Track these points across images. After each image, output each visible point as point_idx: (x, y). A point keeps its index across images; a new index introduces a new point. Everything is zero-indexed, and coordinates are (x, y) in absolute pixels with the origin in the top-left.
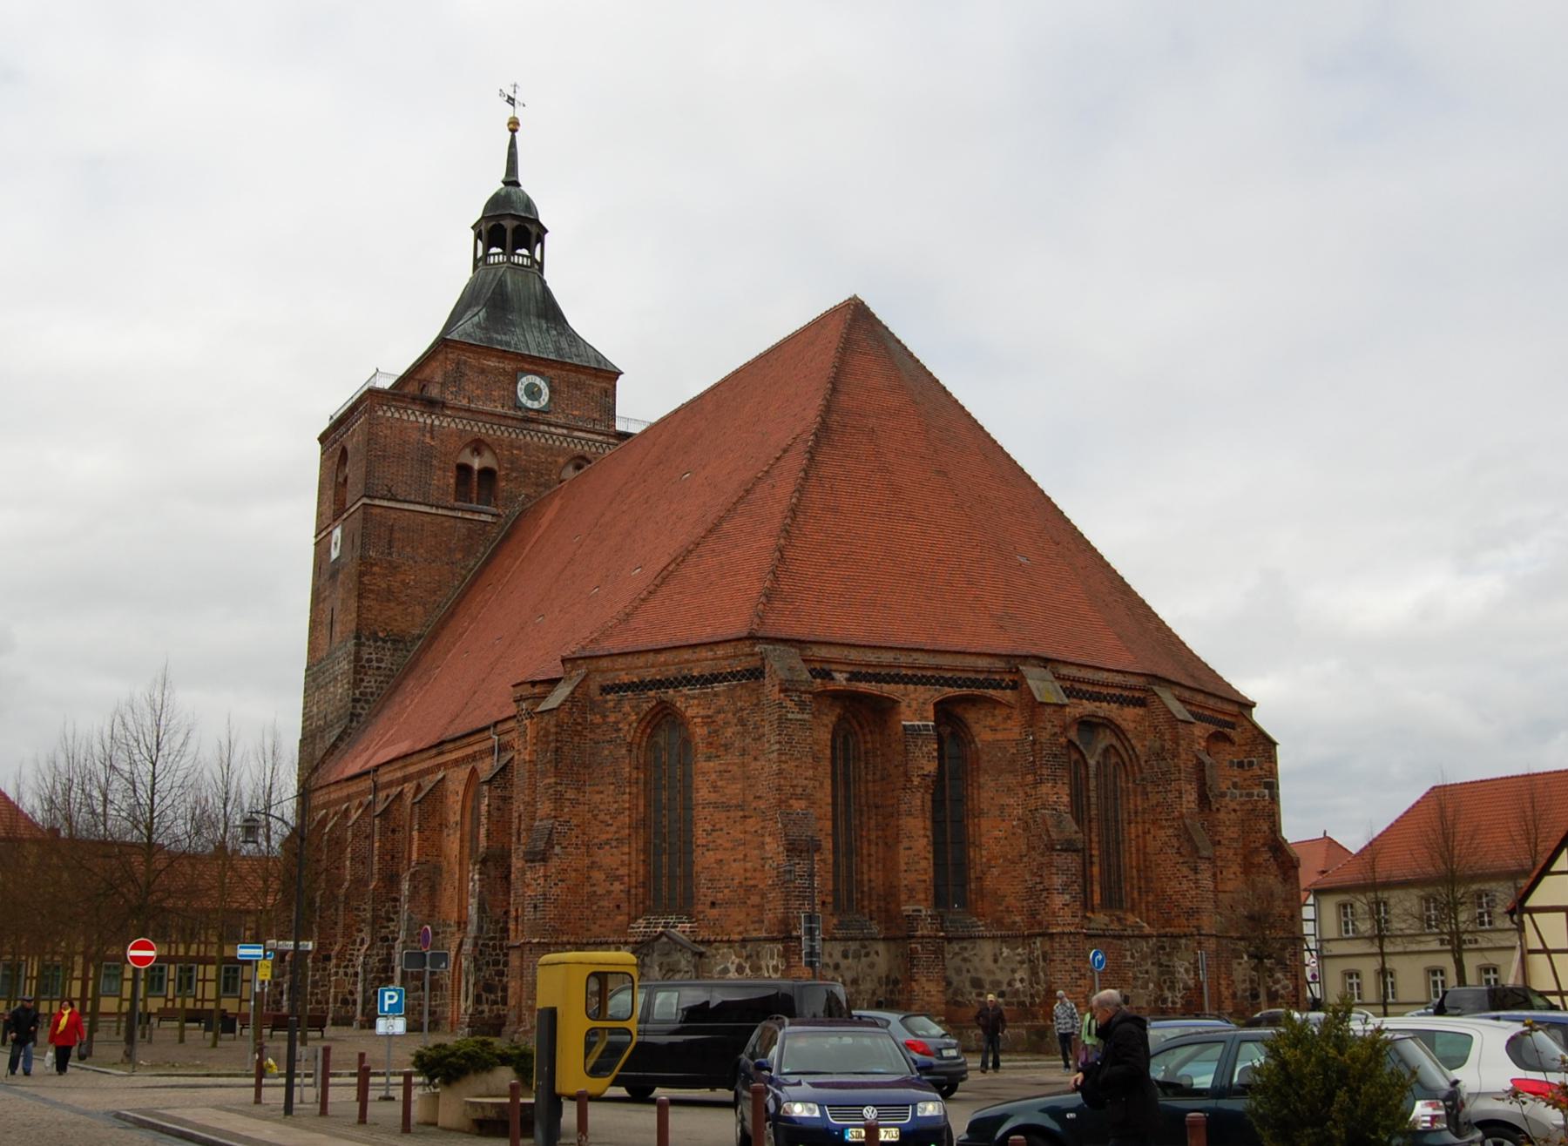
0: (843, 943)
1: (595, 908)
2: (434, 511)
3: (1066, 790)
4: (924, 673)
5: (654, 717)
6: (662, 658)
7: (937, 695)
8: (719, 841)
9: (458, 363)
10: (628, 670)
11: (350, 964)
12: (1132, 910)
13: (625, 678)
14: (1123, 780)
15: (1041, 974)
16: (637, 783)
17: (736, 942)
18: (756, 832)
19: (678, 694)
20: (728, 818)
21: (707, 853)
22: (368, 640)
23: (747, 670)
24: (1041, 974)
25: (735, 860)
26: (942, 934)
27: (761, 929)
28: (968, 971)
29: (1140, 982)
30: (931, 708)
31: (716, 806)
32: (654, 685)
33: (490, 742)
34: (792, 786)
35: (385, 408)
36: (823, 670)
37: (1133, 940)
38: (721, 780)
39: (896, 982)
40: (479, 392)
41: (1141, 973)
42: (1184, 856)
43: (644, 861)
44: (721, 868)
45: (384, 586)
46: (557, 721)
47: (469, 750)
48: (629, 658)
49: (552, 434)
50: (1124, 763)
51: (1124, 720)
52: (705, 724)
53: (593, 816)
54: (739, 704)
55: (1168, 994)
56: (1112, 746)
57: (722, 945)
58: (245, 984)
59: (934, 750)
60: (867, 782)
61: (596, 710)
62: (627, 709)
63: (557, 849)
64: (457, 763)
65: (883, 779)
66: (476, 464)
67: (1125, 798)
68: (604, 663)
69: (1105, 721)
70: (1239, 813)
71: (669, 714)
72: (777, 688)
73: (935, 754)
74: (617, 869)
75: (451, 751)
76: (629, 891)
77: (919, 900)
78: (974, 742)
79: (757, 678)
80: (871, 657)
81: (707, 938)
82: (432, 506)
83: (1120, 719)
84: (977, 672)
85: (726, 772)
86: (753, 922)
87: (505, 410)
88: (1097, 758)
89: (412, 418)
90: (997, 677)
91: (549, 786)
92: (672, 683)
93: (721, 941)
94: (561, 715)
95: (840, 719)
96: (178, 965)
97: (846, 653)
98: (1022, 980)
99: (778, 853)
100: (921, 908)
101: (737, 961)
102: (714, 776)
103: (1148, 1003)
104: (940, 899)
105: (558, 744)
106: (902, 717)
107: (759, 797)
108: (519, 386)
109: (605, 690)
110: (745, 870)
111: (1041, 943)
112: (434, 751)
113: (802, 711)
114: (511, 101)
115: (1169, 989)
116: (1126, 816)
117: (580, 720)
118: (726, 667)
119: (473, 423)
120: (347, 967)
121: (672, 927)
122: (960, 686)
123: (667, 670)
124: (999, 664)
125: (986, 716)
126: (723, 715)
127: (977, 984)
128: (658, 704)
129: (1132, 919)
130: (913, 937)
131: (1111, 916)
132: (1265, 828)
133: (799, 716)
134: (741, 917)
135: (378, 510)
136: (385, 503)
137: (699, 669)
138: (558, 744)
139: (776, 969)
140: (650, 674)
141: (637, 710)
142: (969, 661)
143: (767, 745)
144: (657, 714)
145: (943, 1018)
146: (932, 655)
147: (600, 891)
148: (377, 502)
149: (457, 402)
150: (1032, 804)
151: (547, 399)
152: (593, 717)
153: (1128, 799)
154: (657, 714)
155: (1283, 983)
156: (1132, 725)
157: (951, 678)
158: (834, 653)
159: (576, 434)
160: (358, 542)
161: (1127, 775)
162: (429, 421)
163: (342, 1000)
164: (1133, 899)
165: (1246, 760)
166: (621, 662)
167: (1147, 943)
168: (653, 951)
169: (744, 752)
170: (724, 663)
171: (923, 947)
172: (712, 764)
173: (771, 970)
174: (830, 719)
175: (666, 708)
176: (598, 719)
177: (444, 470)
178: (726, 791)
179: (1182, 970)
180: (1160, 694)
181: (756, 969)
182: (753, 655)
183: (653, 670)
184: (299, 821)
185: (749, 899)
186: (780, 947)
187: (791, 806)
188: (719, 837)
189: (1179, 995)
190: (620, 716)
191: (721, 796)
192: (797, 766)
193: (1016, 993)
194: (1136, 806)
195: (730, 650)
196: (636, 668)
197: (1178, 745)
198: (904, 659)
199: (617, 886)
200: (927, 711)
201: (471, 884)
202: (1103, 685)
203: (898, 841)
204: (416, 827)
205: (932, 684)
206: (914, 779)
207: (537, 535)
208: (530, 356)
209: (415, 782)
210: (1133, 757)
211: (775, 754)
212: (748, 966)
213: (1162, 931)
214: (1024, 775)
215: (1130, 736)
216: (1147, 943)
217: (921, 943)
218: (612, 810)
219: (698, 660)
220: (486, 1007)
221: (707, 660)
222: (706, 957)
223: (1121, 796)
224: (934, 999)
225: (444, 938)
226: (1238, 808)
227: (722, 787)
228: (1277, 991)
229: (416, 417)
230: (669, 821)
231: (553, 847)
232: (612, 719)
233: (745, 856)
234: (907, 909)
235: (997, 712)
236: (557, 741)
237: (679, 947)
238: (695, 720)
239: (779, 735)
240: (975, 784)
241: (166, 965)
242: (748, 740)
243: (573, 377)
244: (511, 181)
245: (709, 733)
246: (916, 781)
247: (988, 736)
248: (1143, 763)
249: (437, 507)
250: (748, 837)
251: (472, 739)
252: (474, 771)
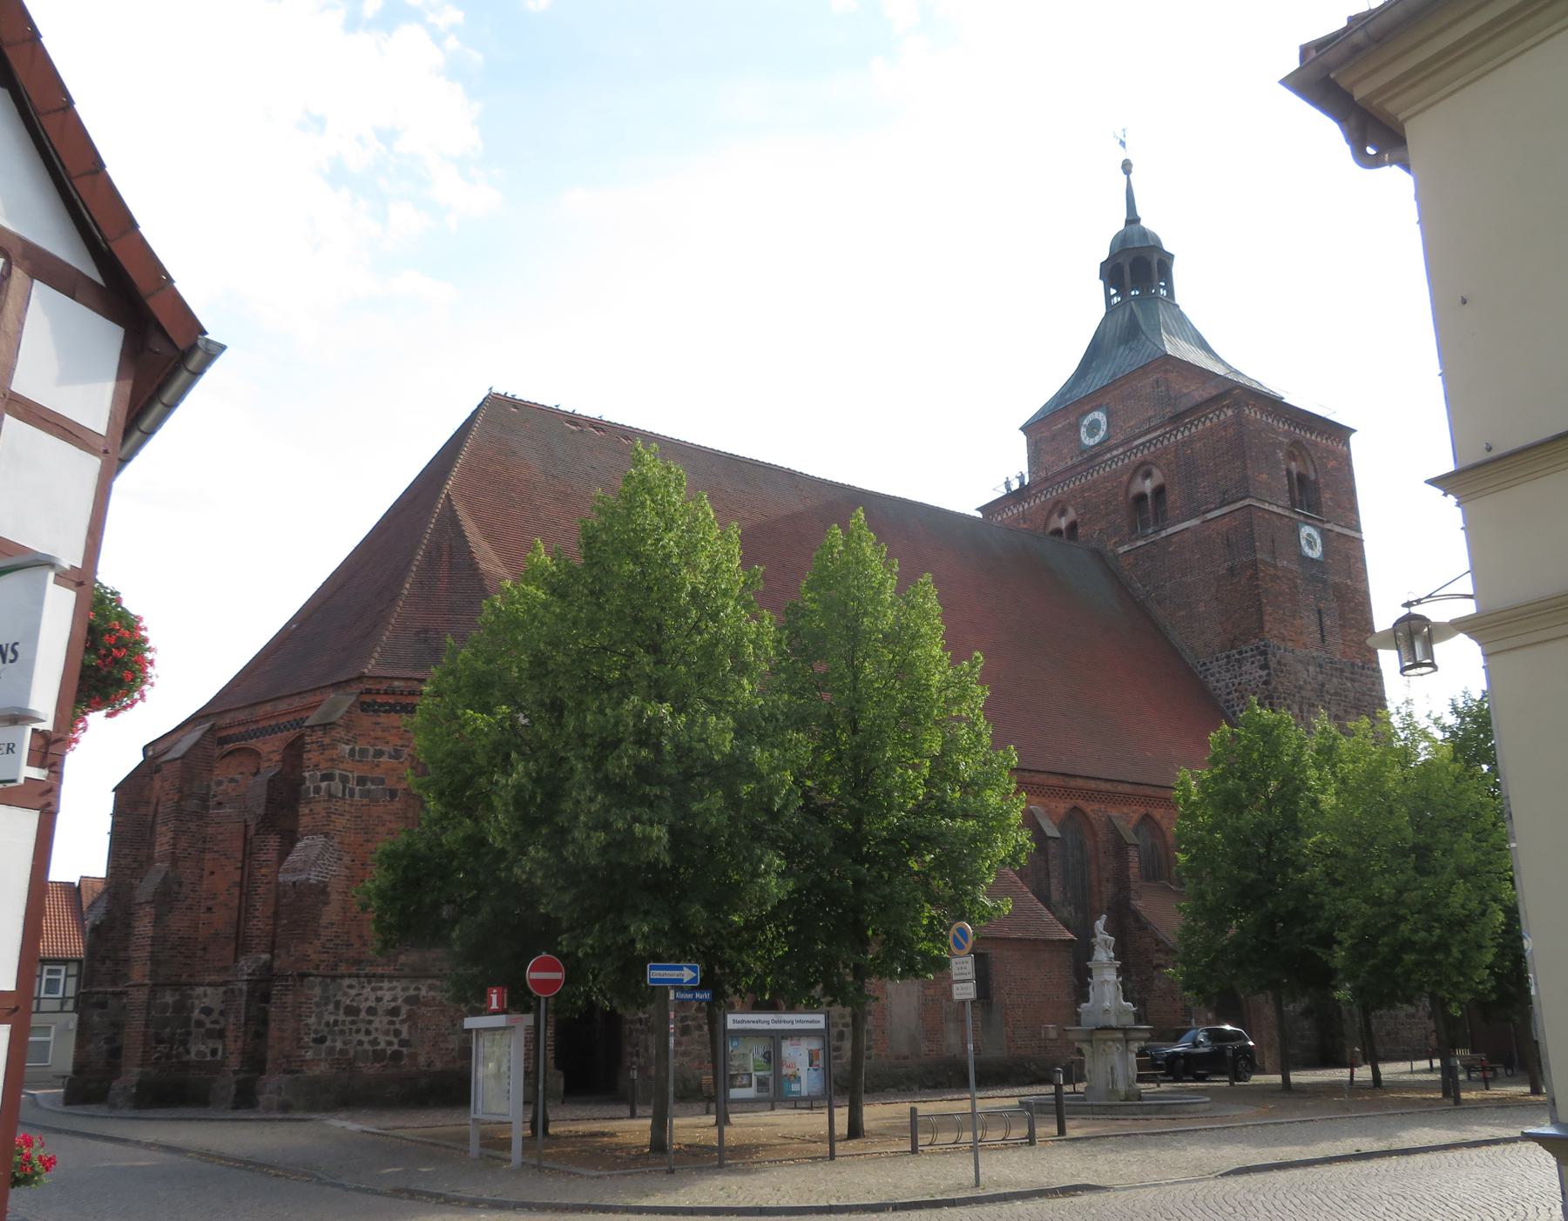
114: (1123, 143)
135: (1280, 503)
151: (1092, 444)
180: (289, 1076)
184: (1132, 908)
244: (1132, 219)
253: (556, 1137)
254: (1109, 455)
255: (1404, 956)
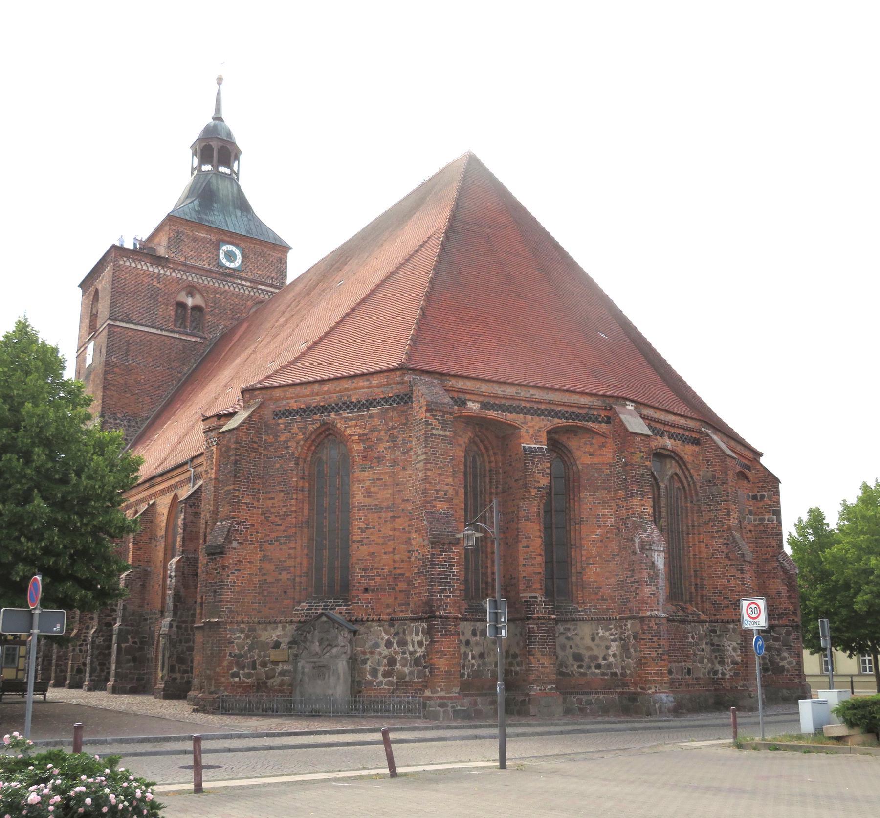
0: (472, 623)
1: (265, 593)
2: (159, 332)
3: (651, 503)
4: (540, 406)
5: (318, 436)
6: (326, 387)
7: (549, 424)
8: (372, 538)
9: (178, 233)
10: (297, 397)
11: (84, 643)
12: (691, 601)
13: (294, 405)
14: (683, 500)
15: (632, 650)
16: (303, 491)
17: (385, 621)
18: (404, 529)
19: (339, 417)
20: (380, 518)
21: (361, 547)
22: (110, 418)
23: (398, 396)
24: (632, 650)
25: (385, 553)
26: (553, 617)
27: (407, 611)
28: (571, 647)
29: (698, 658)
30: (544, 435)
31: (369, 508)
32: (319, 410)
33: (188, 473)
34: (435, 490)
35: (125, 259)
36: (460, 399)
37: (693, 624)
38: (374, 486)
39: (515, 656)
40: (192, 253)
41: (699, 651)
42: (732, 560)
43: (307, 555)
44: (373, 560)
45: (122, 382)
46: (236, 438)
47: (172, 482)
48: (298, 389)
49: (243, 285)
50: (684, 488)
51: (685, 454)
52: (361, 441)
53: (265, 517)
54: (391, 424)
55: (719, 668)
56: (676, 474)
57: (374, 624)
58: (21, 659)
59: (547, 468)
60: (491, 493)
61: (269, 432)
62: (295, 429)
63: (235, 544)
64: (163, 492)
65: (504, 492)
66: (190, 302)
67: (684, 515)
68: (278, 393)
69: (672, 454)
70: (753, 533)
71: (330, 434)
72: (424, 408)
73: (548, 471)
74: (285, 561)
75: (159, 484)
76: (294, 579)
77: (535, 589)
78: (576, 464)
79: (406, 403)
80: (498, 390)
81: (360, 618)
82: (158, 329)
83: (683, 453)
84: (579, 407)
85: (378, 479)
86: (400, 605)
87: (211, 267)
88: (666, 482)
89: (145, 268)
90: (595, 413)
91: (229, 492)
92: (333, 408)
93: (373, 620)
94: (240, 434)
95: (472, 441)
96: (5, 646)
97: (478, 386)
98: (614, 655)
99: (424, 546)
100: (537, 595)
101: (386, 637)
102: (368, 484)
103: (704, 674)
104: (549, 593)
105: (237, 458)
106: (522, 440)
107: (407, 500)
108: (221, 252)
109: (277, 415)
110: (394, 561)
111: (632, 625)
112: (147, 485)
113: (444, 428)
115: (719, 663)
116: (685, 528)
117: (255, 439)
118: (379, 393)
119: (188, 274)
120: (81, 645)
121: (331, 609)
122: (566, 419)
123: (330, 398)
124: (597, 402)
125: (585, 444)
126: (375, 434)
127: (578, 658)
128: (322, 425)
129: (692, 608)
130: (531, 618)
131: (676, 605)
132: (774, 544)
133: (442, 433)
134: (391, 601)
135: (119, 330)
136: (124, 325)
137: (357, 397)
138: (237, 458)
139: (420, 644)
140: (317, 401)
141: (303, 430)
142: (575, 399)
143: (414, 457)
144: (321, 434)
145: (554, 686)
146: (546, 391)
147: (270, 579)
148: (118, 323)
149: (177, 259)
150: (623, 513)
151: (240, 262)
152: (267, 437)
153: (687, 516)
154: (321, 434)
155: (788, 660)
156: (691, 458)
157: (560, 411)
158: (469, 385)
159: (260, 287)
160: (104, 351)
161: (686, 497)
162: (156, 271)
163: (77, 669)
164: (691, 593)
165: (759, 494)
166: (291, 392)
167: (703, 627)
168: (315, 629)
169: (394, 463)
170: (378, 390)
171: (538, 627)
172: (366, 474)
173: (416, 645)
174: (464, 440)
175: (329, 429)
176: (271, 439)
177: (167, 305)
178: (379, 496)
179: (730, 649)
181: (402, 643)
182: (402, 383)
183: (318, 398)
185: (397, 585)
186: (425, 625)
187: (435, 507)
188: (371, 534)
189: (728, 669)
190: (289, 436)
191: (375, 499)
192: (439, 474)
193: (609, 666)
194: (693, 521)
195: (383, 379)
196: (304, 396)
197: (727, 474)
198: (524, 393)
199: (284, 576)
200: (541, 437)
201: (169, 579)
202: (671, 426)
203: (517, 541)
204: (132, 540)
205: (546, 416)
206: (532, 490)
207: (231, 345)
208: (229, 232)
209: (133, 509)
210: (691, 483)
211: (422, 463)
212: (395, 642)
213: (713, 618)
214: (616, 491)
215: (690, 467)
216: (703, 627)
217: (537, 624)
218: (281, 513)
219: (356, 389)
220: (178, 675)
221: (363, 388)
222: (359, 635)
223: (682, 513)
224: (548, 670)
225: (151, 623)
226: (752, 529)
227: (375, 493)
228: (783, 666)
229: (146, 267)
230: (330, 523)
231: (231, 542)
232: (282, 438)
233: (394, 549)
234: (526, 595)
235: (594, 441)
236: (236, 455)
237: (337, 626)
238: (353, 438)
239: (426, 447)
240: (576, 498)
241: (18, 646)
242: (398, 453)
243: (258, 248)
244: (218, 118)
245: (365, 448)
246: (534, 492)
247: (587, 460)
248: (698, 488)
249: (162, 330)
250: (397, 534)
251: (175, 472)
252: (176, 497)
253: (210, 791)
254: (239, 281)
255: (65, 378)
